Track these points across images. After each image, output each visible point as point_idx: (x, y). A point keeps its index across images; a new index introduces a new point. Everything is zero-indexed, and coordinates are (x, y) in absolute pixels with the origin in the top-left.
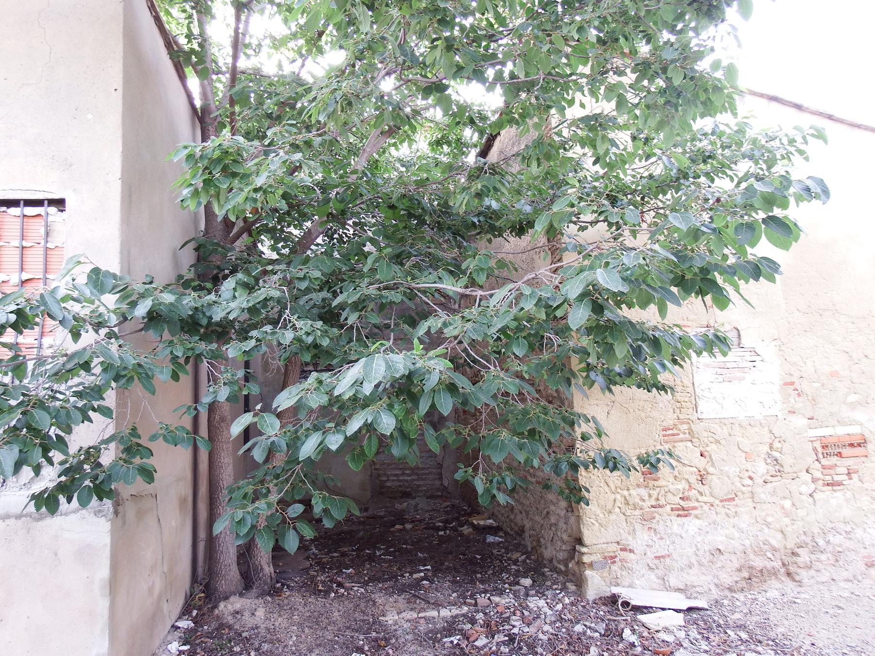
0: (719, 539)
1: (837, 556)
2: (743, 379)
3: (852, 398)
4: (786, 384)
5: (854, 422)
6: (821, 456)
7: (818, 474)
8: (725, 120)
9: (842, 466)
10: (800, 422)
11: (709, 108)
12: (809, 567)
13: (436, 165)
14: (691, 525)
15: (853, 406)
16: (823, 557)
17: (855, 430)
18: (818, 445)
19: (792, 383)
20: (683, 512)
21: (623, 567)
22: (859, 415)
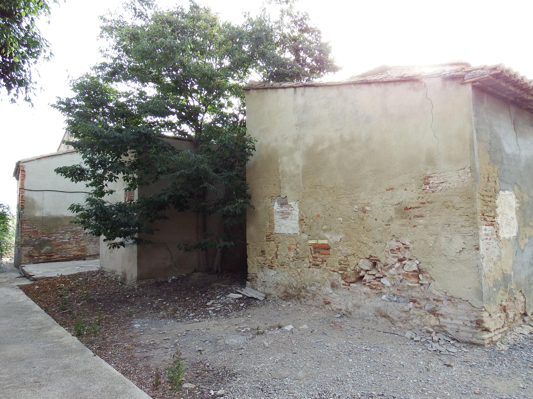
0: (279, 278)
1: (314, 295)
2: (288, 217)
3: (325, 227)
4: (301, 220)
5: (326, 239)
6: (313, 252)
7: (311, 260)
8: (71, 118)
9: (320, 257)
10: (305, 236)
11: (71, 120)
12: (304, 298)
13: (320, 362)
14: (273, 272)
15: (325, 231)
16: (309, 295)
17: (325, 242)
18: (311, 247)
19: (303, 220)
20: (271, 267)
21: (256, 283)
22: (327, 236)
